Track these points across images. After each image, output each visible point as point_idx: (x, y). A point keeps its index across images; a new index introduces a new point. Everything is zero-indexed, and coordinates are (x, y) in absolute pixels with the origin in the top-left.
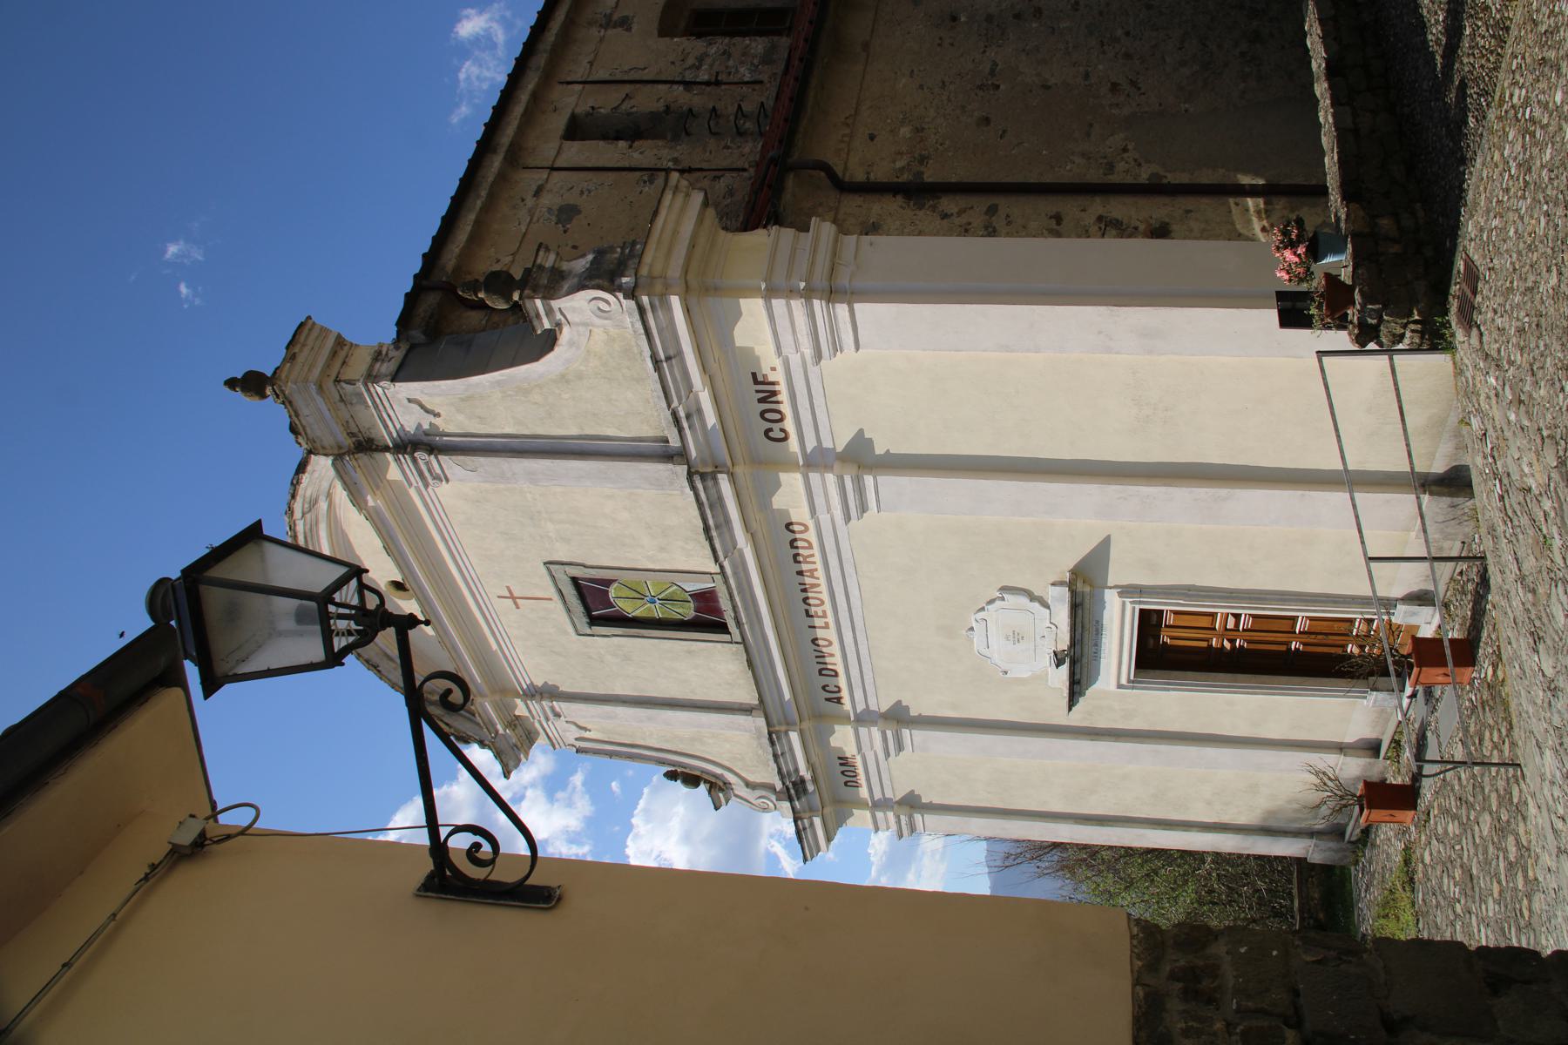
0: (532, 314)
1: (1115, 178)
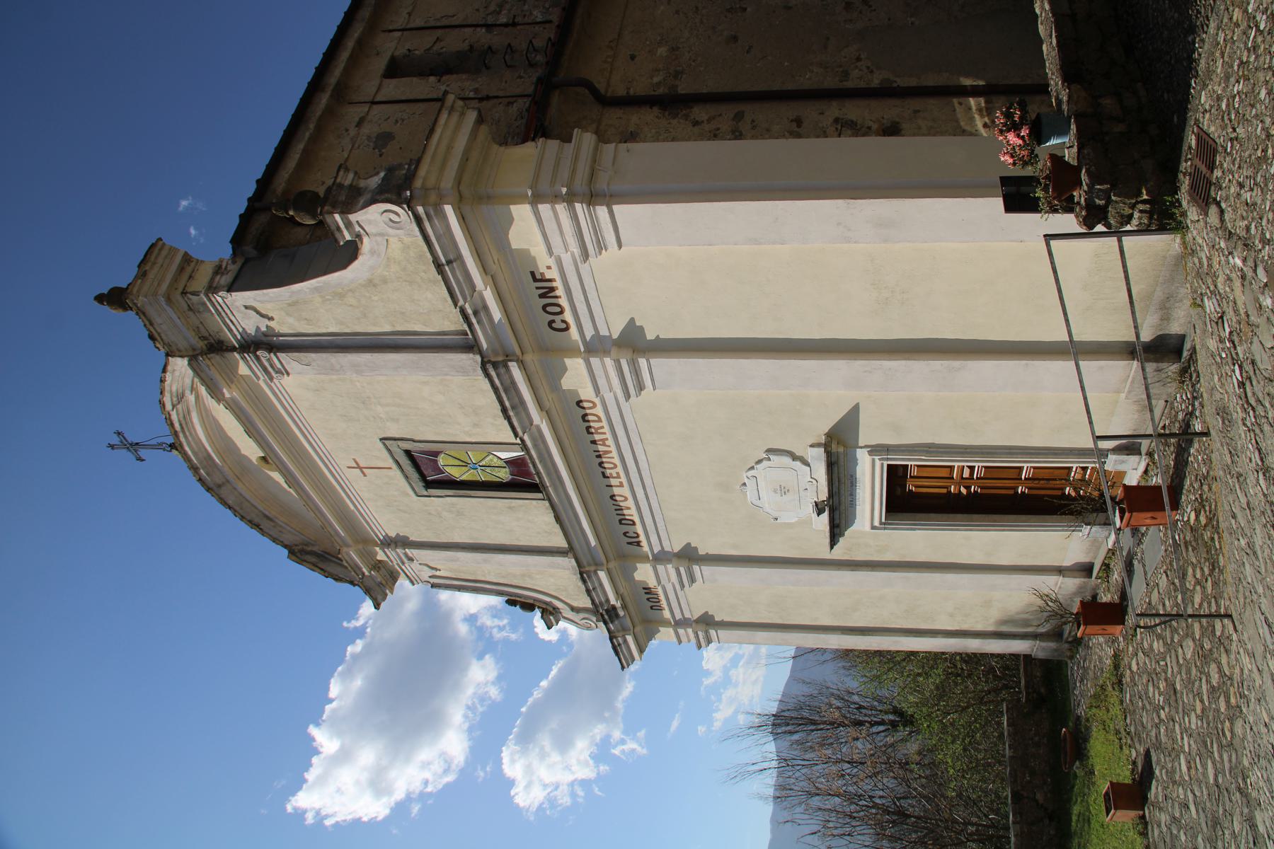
0: (333, 228)
1: (849, 84)
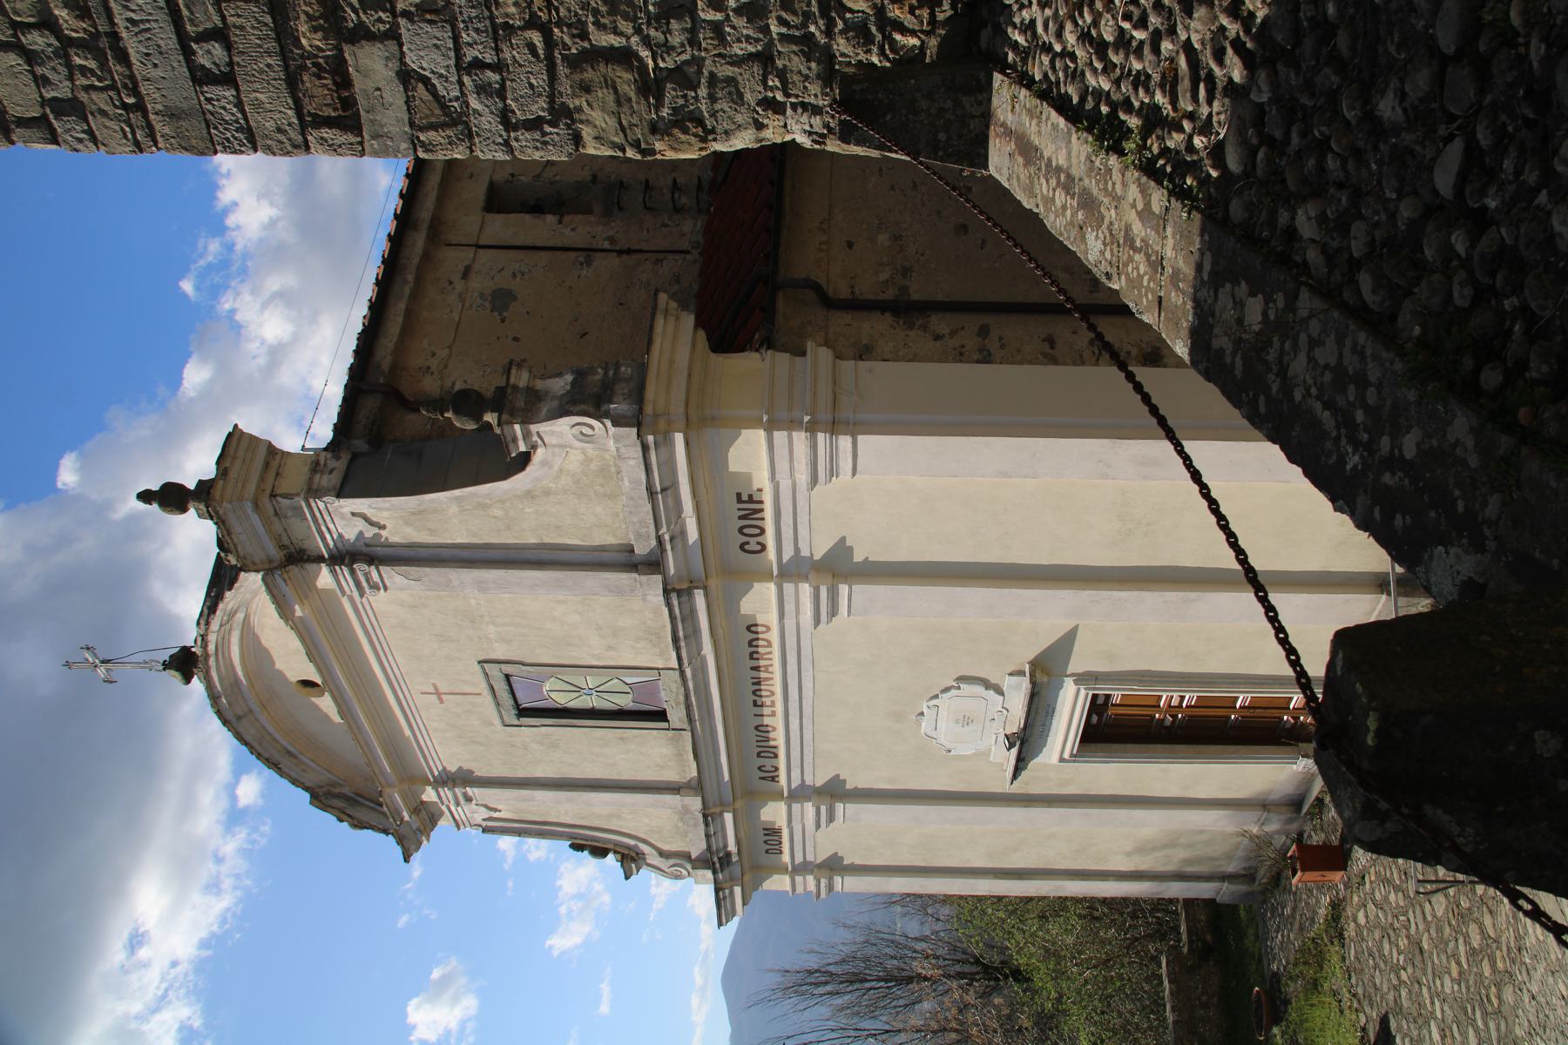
0: (509, 439)
